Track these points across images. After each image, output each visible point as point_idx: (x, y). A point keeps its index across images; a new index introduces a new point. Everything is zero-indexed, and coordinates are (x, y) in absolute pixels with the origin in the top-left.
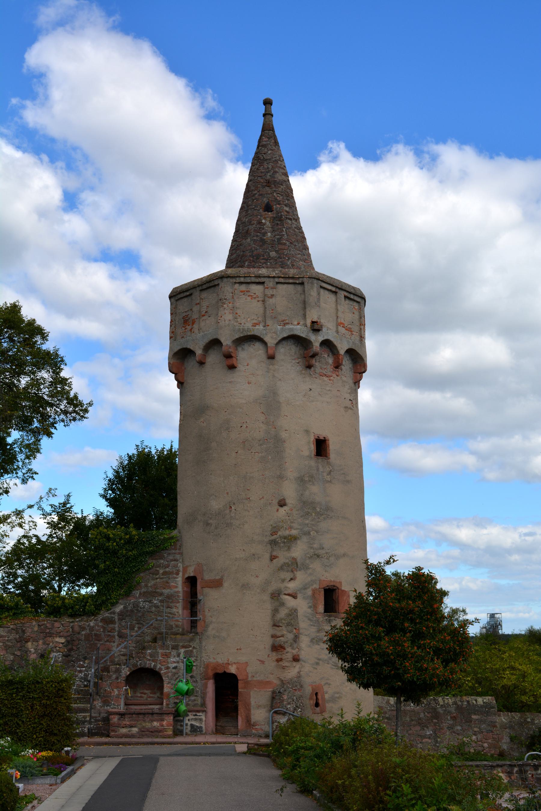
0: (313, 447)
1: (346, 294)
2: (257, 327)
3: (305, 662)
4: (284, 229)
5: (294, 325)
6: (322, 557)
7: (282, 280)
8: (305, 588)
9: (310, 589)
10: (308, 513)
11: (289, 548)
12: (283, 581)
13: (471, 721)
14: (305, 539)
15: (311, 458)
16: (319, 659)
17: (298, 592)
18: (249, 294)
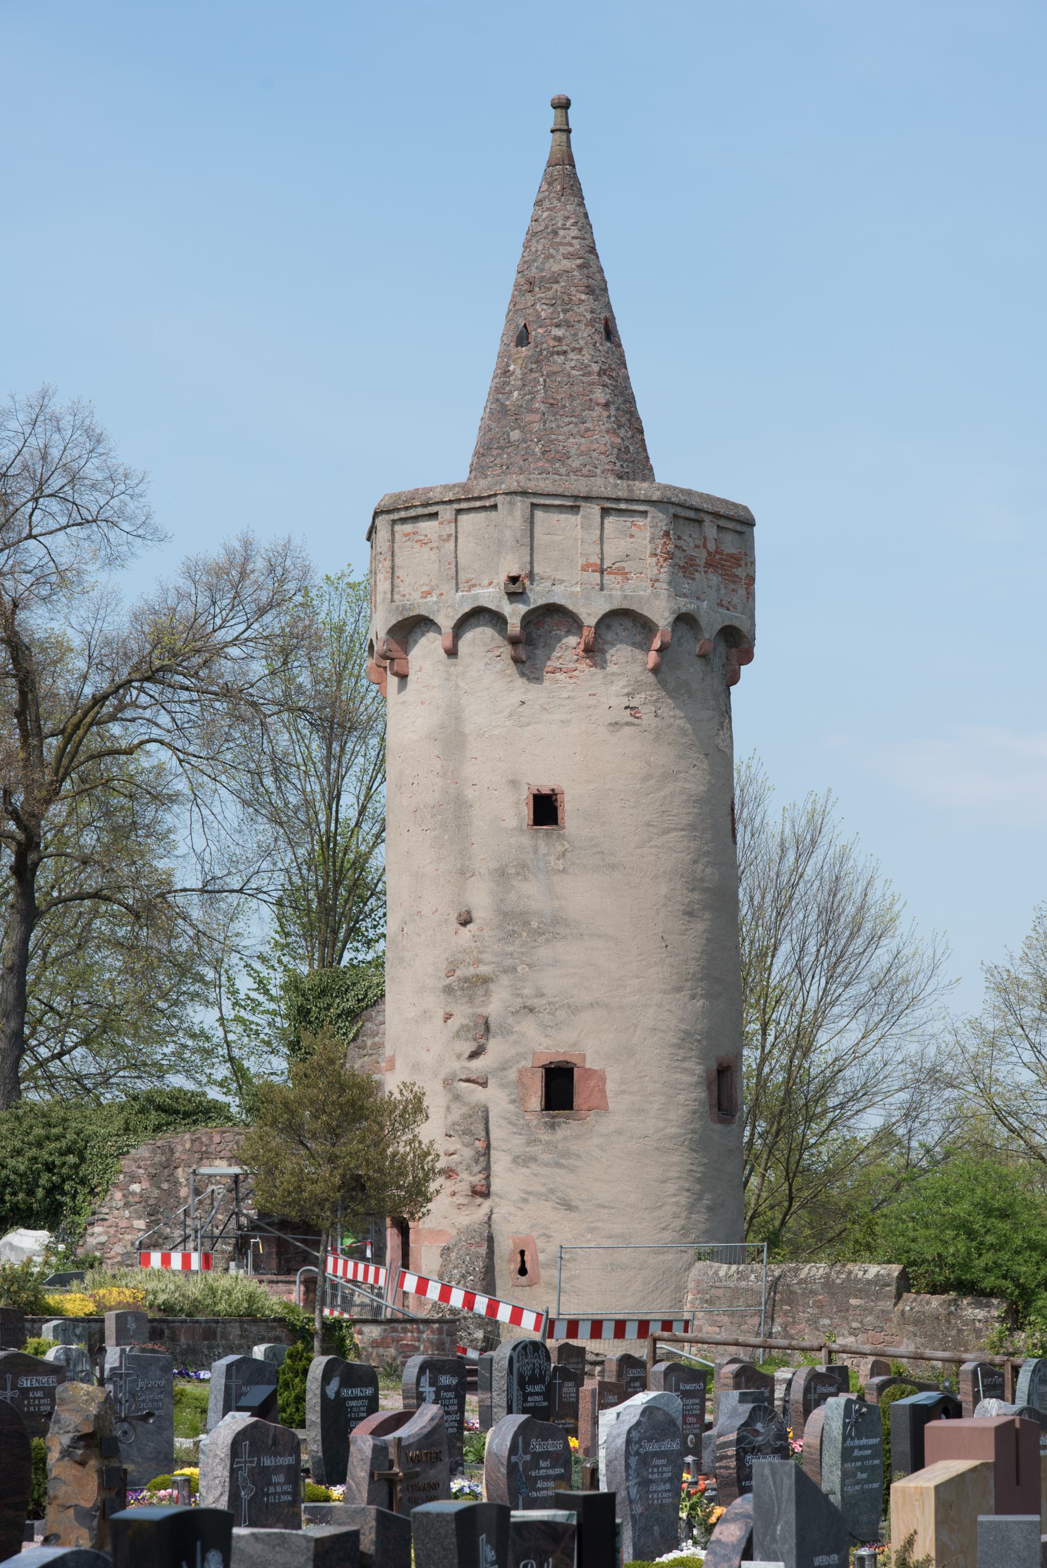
0: (527, 812)
2: (429, 599)
3: (501, 1197)
4: (541, 379)
5: (483, 587)
6: (539, 1012)
9: (514, 1069)
10: (512, 934)
13: (847, 1310)
15: (522, 831)
16: (530, 1193)
17: (489, 1076)
18: (417, 537)
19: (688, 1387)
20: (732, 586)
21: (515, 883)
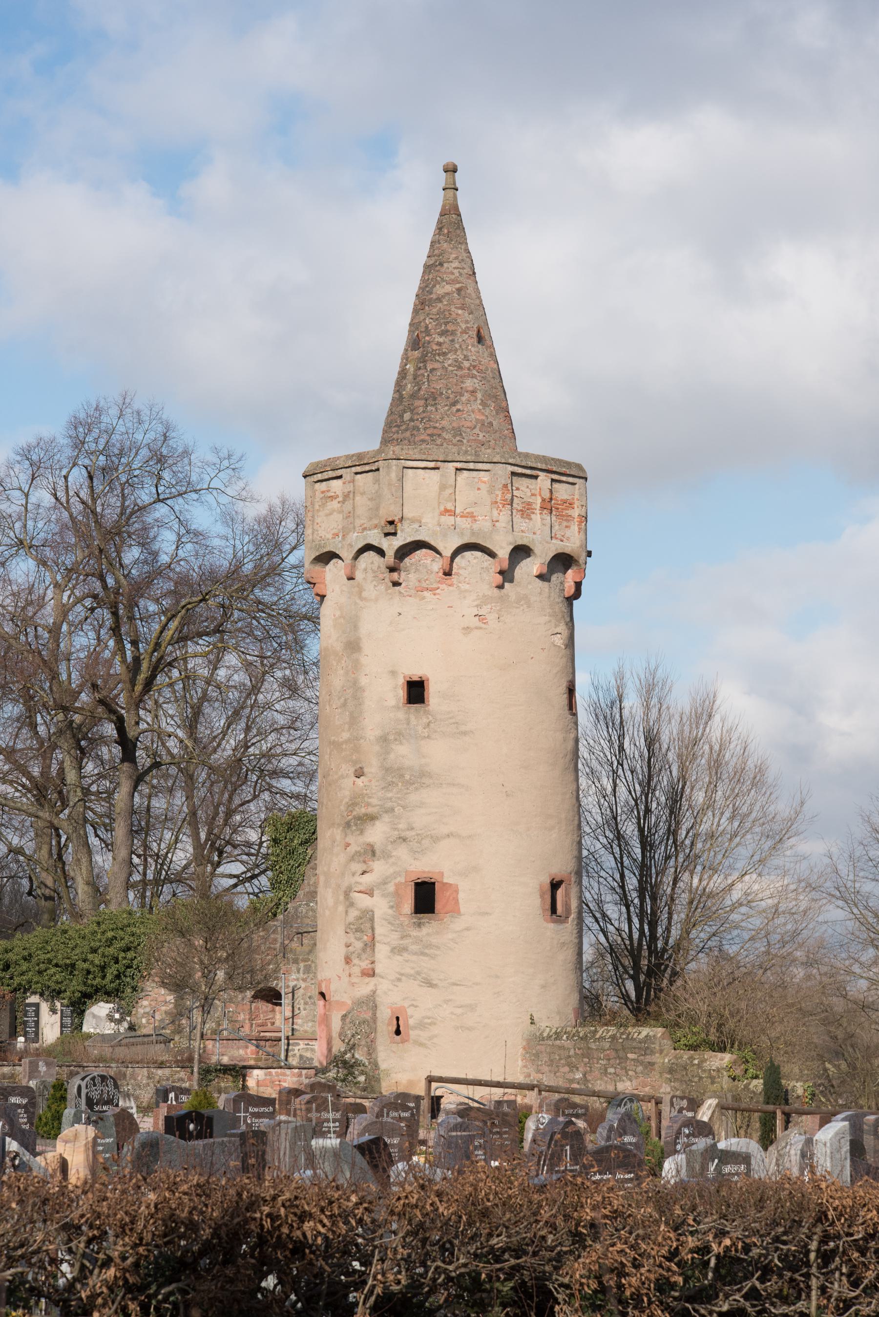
1: (459, 465)
7: (359, 469)
8: (385, 883)
11: (362, 832)
12: (354, 874)
14: (386, 818)
16: (402, 975)
19: (256, 1110)
20: (565, 524)
21: (393, 747)
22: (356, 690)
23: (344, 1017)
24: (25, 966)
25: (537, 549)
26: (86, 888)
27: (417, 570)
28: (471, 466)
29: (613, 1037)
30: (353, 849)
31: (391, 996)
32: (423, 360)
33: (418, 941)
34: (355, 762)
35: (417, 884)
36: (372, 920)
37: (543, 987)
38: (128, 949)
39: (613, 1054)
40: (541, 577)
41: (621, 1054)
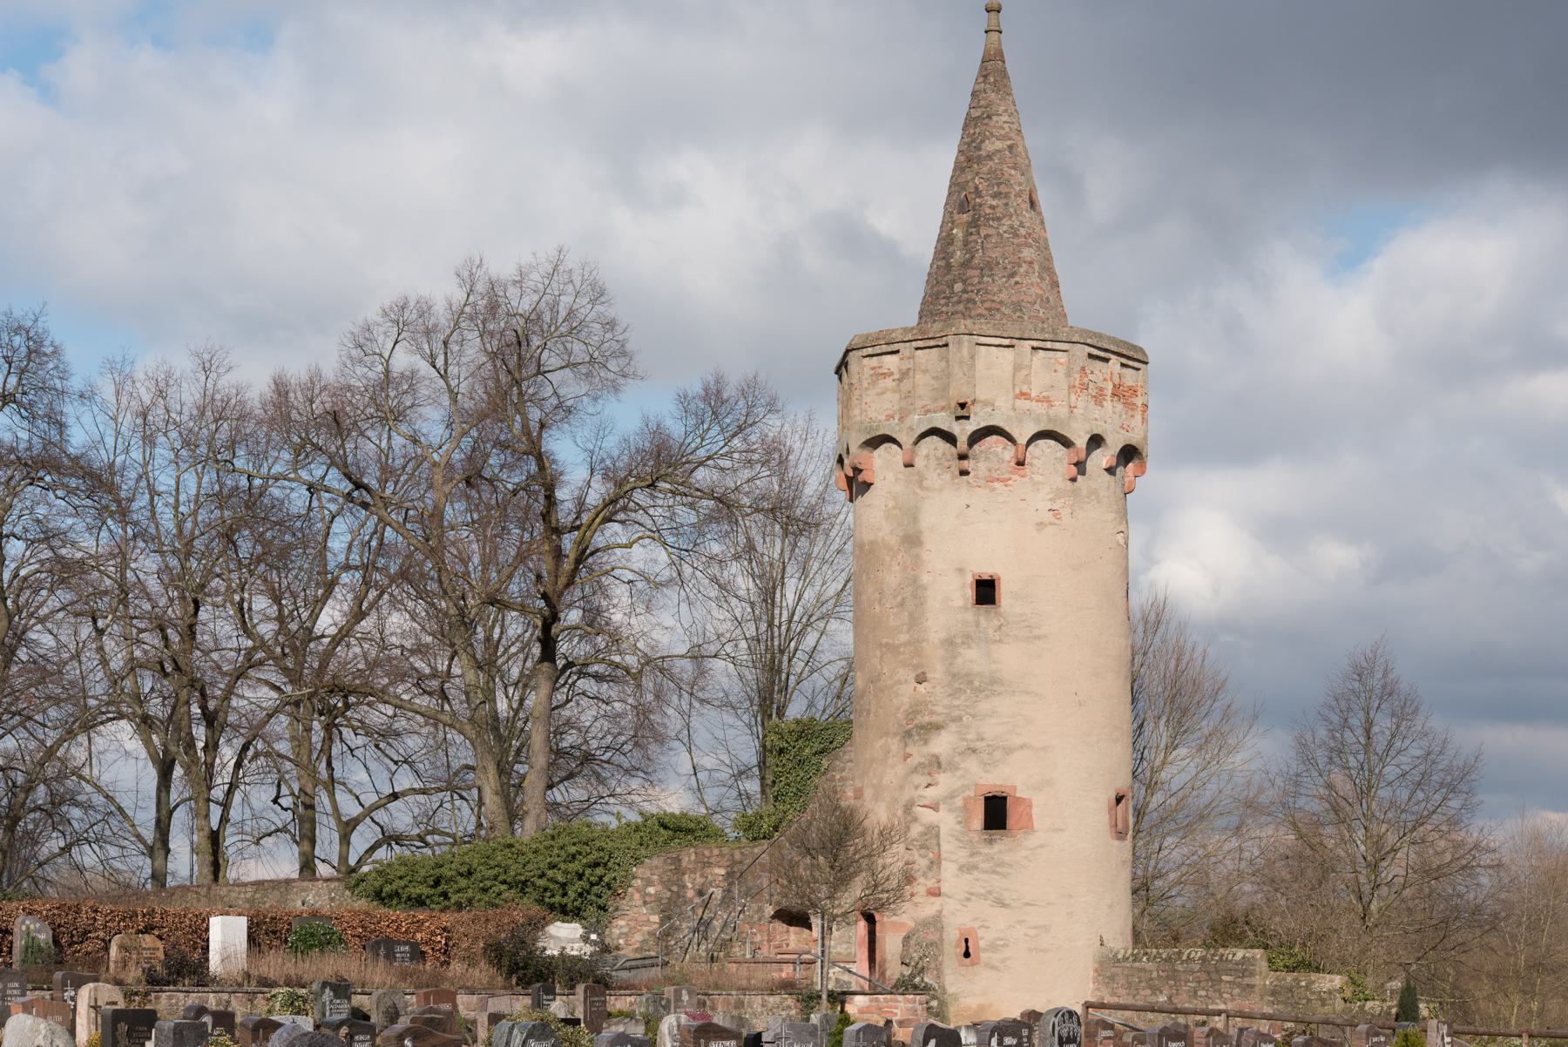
0: (970, 593)
1: (1035, 344)
7: (921, 344)
11: (926, 742)
12: (917, 787)
14: (953, 727)
22: (916, 590)
23: (907, 939)
24: (463, 882)
25: (1109, 439)
26: (496, 798)
27: (987, 458)
28: (1049, 345)
29: (1203, 959)
30: (914, 760)
31: (957, 918)
32: (974, 224)
33: (990, 858)
34: (916, 667)
35: (987, 799)
36: (938, 836)
37: (1110, 907)
38: (596, 865)
39: (1204, 976)
40: (1110, 471)
41: (1214, 976)
